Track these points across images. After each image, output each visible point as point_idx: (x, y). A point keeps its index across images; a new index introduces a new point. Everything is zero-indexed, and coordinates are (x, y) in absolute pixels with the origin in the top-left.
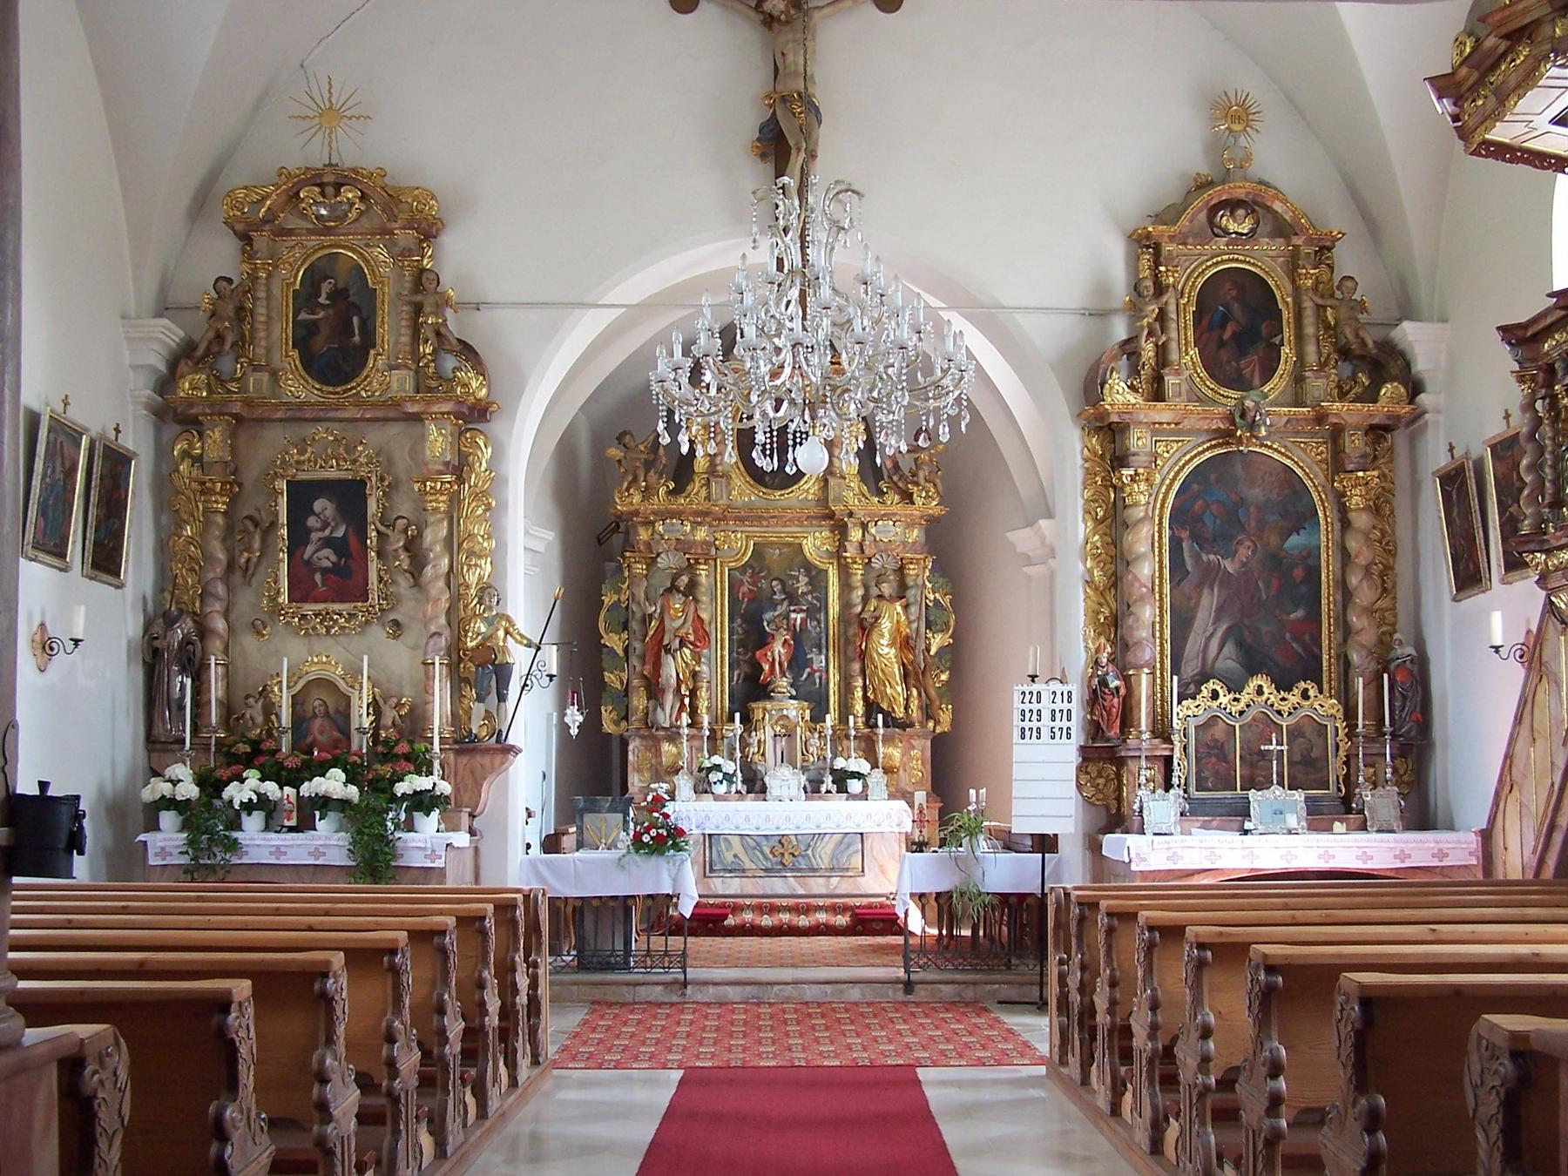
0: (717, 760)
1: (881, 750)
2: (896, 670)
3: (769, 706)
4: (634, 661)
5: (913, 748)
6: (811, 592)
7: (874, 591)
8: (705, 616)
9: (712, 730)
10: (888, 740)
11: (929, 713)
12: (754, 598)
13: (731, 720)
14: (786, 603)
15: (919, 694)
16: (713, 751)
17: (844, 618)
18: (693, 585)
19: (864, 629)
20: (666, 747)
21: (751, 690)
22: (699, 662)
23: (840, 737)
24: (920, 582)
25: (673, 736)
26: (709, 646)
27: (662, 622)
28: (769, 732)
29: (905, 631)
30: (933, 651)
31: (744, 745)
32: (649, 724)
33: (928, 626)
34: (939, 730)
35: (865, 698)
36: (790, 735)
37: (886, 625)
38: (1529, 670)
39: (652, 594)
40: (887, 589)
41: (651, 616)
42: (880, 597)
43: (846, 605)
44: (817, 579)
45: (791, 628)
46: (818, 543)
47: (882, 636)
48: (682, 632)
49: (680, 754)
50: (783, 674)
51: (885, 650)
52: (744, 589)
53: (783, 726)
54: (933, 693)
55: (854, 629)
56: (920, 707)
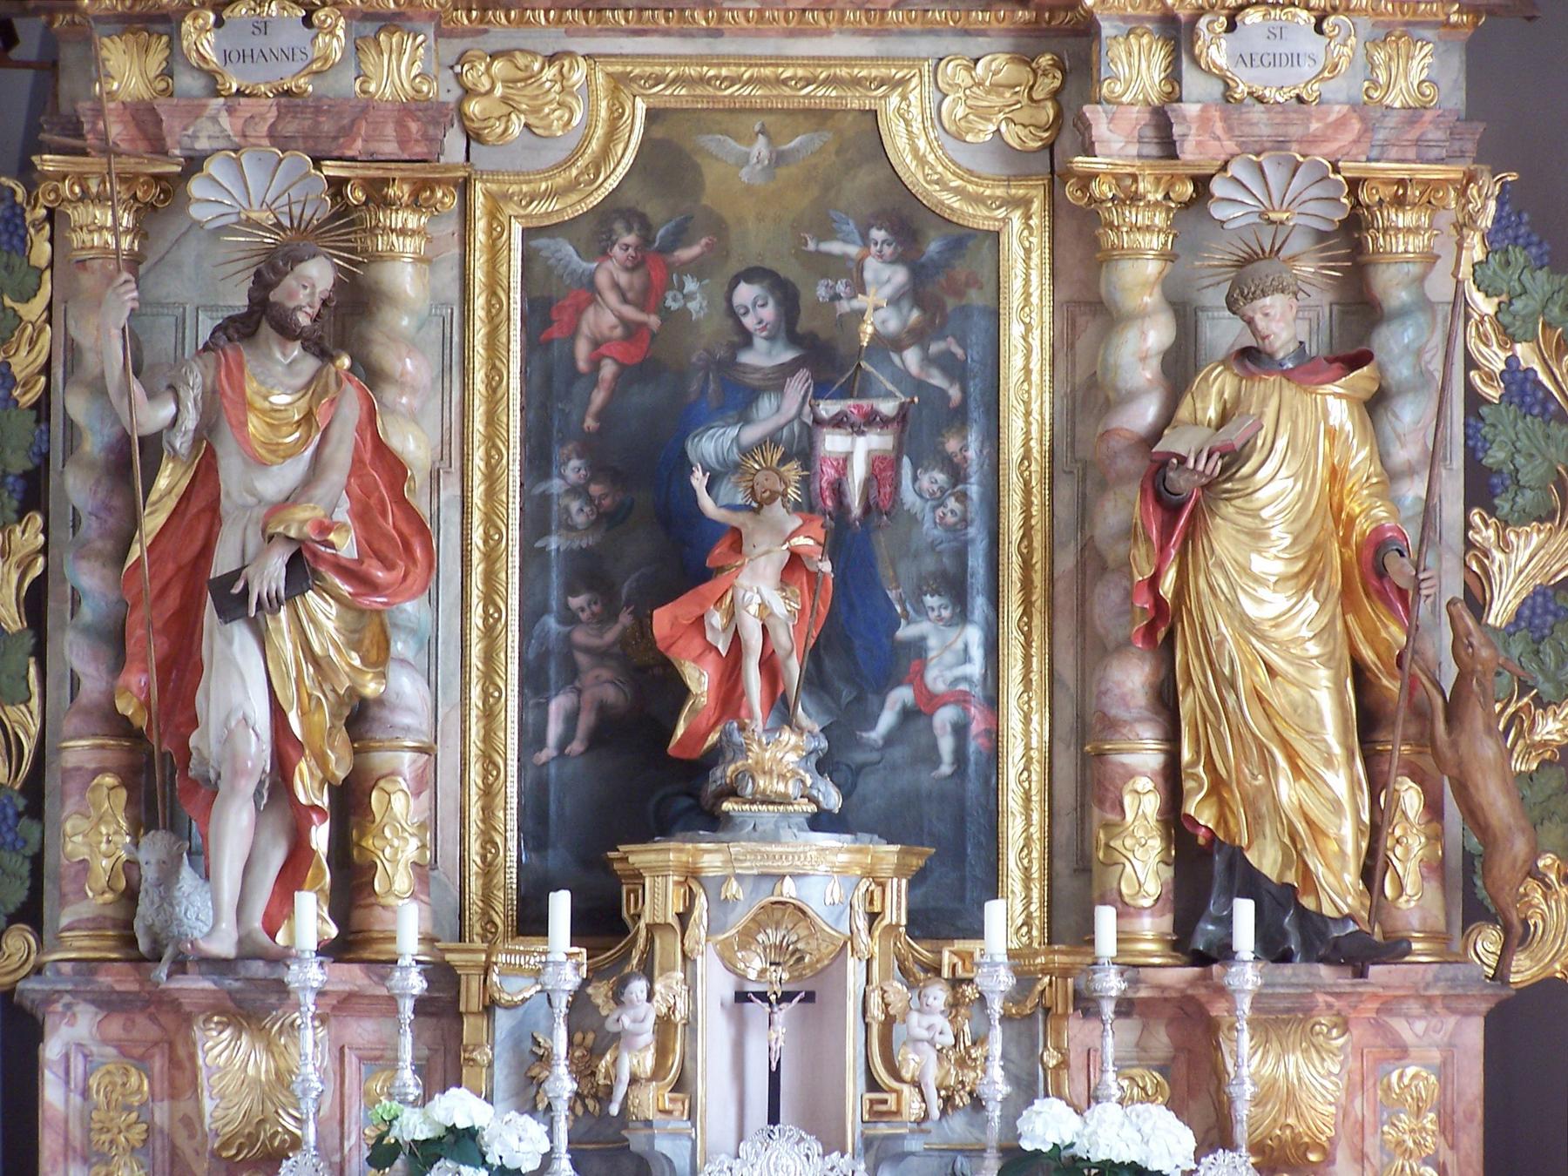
0: (458, 1107)
1: (1249, 1064)
2: (1324, 700)
3: (711, 857)
4: (74, 652)
5: (1401, 1052)
6: (918, 336)
7: (1223, 332)
8: (412, 444)
9: (441, 975)
10: (1280, 1019)
11: (1475, 894)
12: (649, 358)
13: (532, 922)
14: (797, 387)
15: (1434, 809)
16: (444, 1067)
17: (1075, 460)
18: (355, 302)
19: (1167, 504)
20: (224, 1055)
21: (626, 784)
22: (379, 658)
23: (1048, 1004)
24: (1440, 287)
25: (253, 991)
26: (429, 585)
27: (206, 470)
28: (716, 984)
29: (1369, 513)
30: (1500, 612)
31: (593, 1039)
32: (137, 935)
33: (1481, 488)
34: (1524, 970)
35: (1174, 821)
36: (808, 994)
37: (1276, 488)
38: (94, 919)
39: (161, 344)
40: (1283, 322)
41: (153, 447)
42: (1252, 357)
43: (1085, 395)
44: (946, 270)
45: (823, 502)
46: (954, 109)
47: (1258, 536)
48: (299, 522)
49: (283, 1079)
50: (781, 710)
51: (1267, 600)
52: (603, 319)
53: (782, 954)
54: (1497, 803)
55: (1122, 507)
56: (1437, 869)
